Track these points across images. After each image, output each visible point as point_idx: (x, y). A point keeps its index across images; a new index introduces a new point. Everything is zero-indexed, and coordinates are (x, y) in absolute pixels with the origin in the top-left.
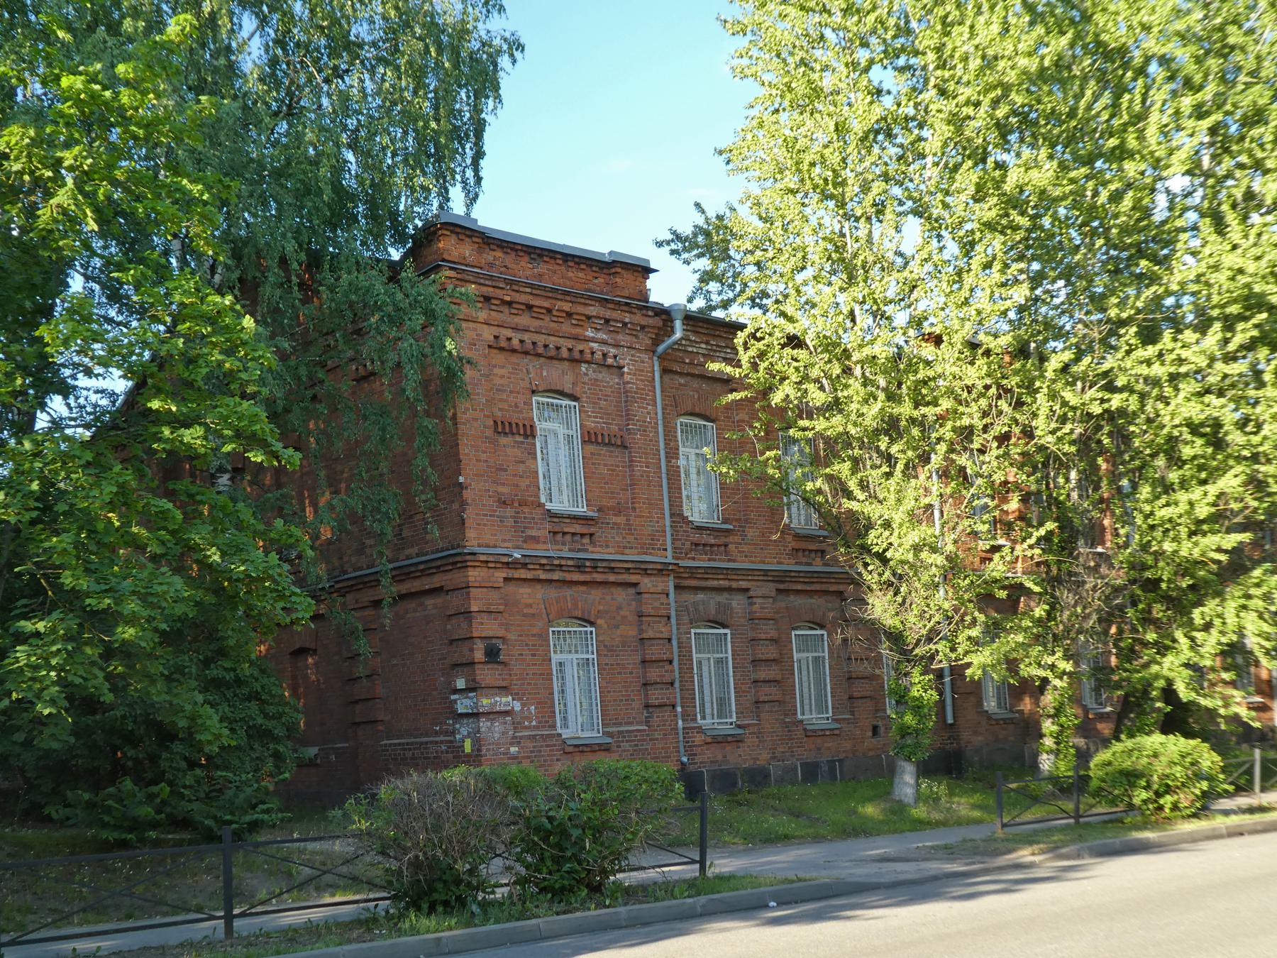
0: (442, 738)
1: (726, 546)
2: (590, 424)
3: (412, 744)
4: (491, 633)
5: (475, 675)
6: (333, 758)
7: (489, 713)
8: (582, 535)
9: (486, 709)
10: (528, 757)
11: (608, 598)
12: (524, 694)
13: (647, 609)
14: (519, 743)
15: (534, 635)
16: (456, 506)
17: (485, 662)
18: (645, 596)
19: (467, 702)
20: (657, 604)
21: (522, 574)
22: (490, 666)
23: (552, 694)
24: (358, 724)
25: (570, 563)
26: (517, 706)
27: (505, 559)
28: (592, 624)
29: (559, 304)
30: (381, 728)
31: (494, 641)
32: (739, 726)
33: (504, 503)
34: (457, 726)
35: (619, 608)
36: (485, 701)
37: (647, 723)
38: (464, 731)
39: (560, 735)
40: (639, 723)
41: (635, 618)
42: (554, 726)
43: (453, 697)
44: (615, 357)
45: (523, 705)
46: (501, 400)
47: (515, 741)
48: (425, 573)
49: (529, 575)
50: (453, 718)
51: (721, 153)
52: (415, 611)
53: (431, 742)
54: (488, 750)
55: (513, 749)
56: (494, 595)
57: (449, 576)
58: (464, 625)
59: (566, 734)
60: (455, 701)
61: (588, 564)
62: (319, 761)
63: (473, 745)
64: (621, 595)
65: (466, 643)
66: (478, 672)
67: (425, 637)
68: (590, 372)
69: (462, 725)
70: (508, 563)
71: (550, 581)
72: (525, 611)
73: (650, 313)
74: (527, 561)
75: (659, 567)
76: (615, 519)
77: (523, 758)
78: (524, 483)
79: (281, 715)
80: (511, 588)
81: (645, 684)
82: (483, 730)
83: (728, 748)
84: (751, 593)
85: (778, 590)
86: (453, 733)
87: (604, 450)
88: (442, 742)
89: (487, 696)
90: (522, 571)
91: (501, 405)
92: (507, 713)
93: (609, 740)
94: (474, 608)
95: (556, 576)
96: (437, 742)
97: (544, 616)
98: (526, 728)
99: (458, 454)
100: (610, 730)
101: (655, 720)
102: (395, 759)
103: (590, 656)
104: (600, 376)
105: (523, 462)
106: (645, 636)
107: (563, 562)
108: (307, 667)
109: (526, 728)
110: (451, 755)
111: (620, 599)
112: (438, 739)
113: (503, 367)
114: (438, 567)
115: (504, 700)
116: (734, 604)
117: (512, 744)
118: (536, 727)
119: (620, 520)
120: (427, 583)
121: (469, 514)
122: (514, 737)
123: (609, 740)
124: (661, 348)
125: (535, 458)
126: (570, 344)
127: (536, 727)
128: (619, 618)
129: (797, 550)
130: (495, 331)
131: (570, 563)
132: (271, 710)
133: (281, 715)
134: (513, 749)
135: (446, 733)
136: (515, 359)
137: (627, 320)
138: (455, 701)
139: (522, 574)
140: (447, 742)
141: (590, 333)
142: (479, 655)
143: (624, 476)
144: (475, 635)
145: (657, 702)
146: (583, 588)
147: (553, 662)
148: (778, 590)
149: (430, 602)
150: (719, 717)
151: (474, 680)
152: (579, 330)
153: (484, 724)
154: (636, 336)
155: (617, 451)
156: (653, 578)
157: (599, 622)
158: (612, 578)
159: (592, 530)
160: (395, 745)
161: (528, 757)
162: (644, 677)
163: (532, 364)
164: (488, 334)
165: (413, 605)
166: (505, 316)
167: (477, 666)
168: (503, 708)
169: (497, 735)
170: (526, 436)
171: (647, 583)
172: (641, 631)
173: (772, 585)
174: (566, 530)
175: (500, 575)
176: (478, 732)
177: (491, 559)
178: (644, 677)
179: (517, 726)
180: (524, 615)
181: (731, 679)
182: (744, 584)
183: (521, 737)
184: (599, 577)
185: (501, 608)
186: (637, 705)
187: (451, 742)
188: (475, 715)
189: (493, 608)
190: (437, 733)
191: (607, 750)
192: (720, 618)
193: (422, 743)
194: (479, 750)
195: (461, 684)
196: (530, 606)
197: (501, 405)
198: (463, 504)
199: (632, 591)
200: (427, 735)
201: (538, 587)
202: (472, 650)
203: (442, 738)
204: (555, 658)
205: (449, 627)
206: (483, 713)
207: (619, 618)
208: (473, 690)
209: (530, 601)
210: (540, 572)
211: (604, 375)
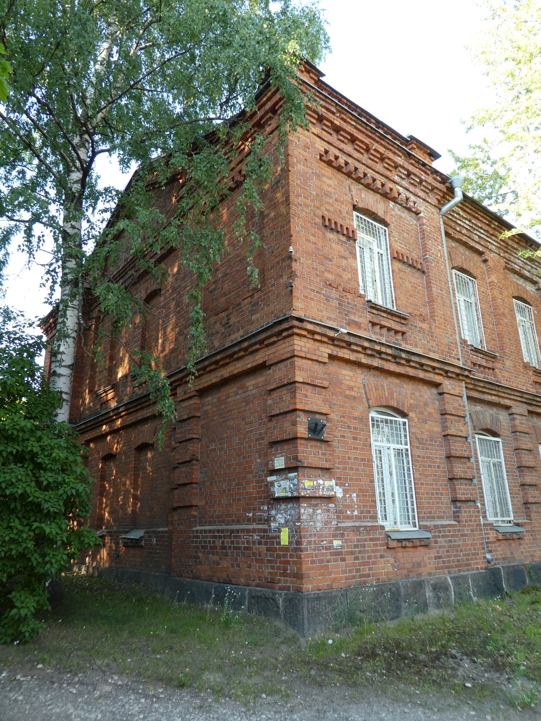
0: (254, 526)
1: (493, 369)
2: (397, 247)
3: (222, 531)
4: (315, 408)
5: (296, 451)
6: (154, 540)
7: (311, 498)
8: (396, 332)
9: (308, 493)
10: (352, 553)
11: (417, 394)
12: (346, 479)
13: (450, 408)
14: (342, 535)
15: (355, 418)
16: (284, 280)
17: (308, 439)
18: (446, 395)
19: (286, 484)
20: (456, 405)
21: (345, 354)
22: (312, 443)
23: (373, 481)
24: (175, 509)
25: (389, 351)
26: (339, 492)
27: (331, 334)
28: (404, 415)
29: (376, 146)
30: (194, 513)
31: (318, 416)
32: (518, 525)
33: (330, 285)
34: (273, 512)
35: (426, 404)
36: (308, 483)
37: (456, 517)
38: (281, 519)
39: (383, 527)
40: (448, 518)
41: (437, 416)
42: (374, 518)
43: (270, 479)
44: (415, 203)
45: (345, 491)
46: (328, 203)
47: (339, 533)
48: (249, 352)
49: (353, 357)
50: (269, 504)
51: (463, 123)
52: (236, 394)
53: (243, 530)
54: (309, 543)
55: (337, 543)
56: (316, 367)
57: (272, 349)
58: (287, 397)
59: (388, 526)
60: (272, 484)
61: (403, 355)
62: (143, 543)
63: (291, 536)
64: (428, 393)
65: (288, 416)
66: (300, 448)
67: (244, 419)
68: (396, 209)
69: (278, 511)
70: (332, 339)
71: (369, 367)
72: (347, 392)
73: (439, 178)
74: (352, 340)
75: (457, 371)
76: (420, 324)
77: (348, 553)
78: (346, 276)
79: (59, 485)
80: (334, 367)
81: (451, 479)
82: (304, 517)
83: (513, 545)
84: (513, 410)
85: (530, 412)
86: (268, 521)
87: (408, 270)
88: (254, 531)
89: (309, 478)
90: (346, 351)
91: (328, 207)
92: (329, 499)
93: (428, 535)
94: (299, 378)
95: (376, 362)
96: (248, 531)
97: (365, 400)
98: (348, 518)
99: (289, 229)
100: (428, 523)
101: (464, 515)
102: (204, 547)
103: (403, 447)
104: (403, 215)
105: (346, 259)
106: (450, 432)
107: (383, 349)
108: (146, 460)
109: (348, 518)
110: (264, 547)
111: (426, 397)
112: (250, 527)
113: (331, 179)
114: (261, 342)
115: (327, 483)
116: (501, 417)
117: (335, 536)
118: (358, 518)
119: (425, 326)
120: (249, 362)
121: (297, 284)
122: (338, 528)
123: (428, 535)
124: (445, 209)
125: (355, 258)
126: (383, 180)
127: (358, 518)
128: (426, 414)
129: (536, 382)
130: (327, 147)
131: (389, 351)
132: (47, 477)
133: (59, 485)
134: (337, 543)
135: (260, 520)
136: (340, 176)
137: (423, 178)
138: (272, 484)
139: (345, 354)
140: (260, 530)
141: (396, 178)
142: (302, 430)
143: (424, 295)
144: (299, 406)
145: (463, 497)
146: (396, 381)
147: (373, 448)
148: (530, 412)
149: (251, 383)
150: (502, 516)
151: (296, 458)
152: (388, 173)
153: (305, 510)
154: (427, 193)
155: (418, 274)
156: (451, 381)
157: (412, 414)
158: (421, 374)
159: (404, 329)
160: (206, 531)
161: (352, 553)
162: (451, 471)
163: (356, 188)
164: (321, 146)
165: (235, 389)
166: (334, 138)
167: (299, 441)
168: (326, 493)
169: (319, 525)
170: (349, 238)
171: (448, 385)
172: (445, 428)
173: (525, 406)
174: (383, 323)
175: (325, 350)
176: (299, 520)
177: (318, 329)
178: (451, 471)
179: (340, 515)
180: (346, 397)
181: (506, 482)
182: (508, 402)
183: (345, 529)
184: (411, 372)
185: (326, 384)
186: (446, 499)
187: (265, 531)
188: (296, 499)
189: (317, 382)
190: (249, 521)
191: (426, 546)
192: (494, 429)
193: (232, 531)
194: (299, 543)
195: (279, 463)
196: (351, 388)
197: (328, 207)
198: (292, 275)
199: (434, 391)
200: (239, 522)
201: (359, 371)
202: (294, 423)
203: (254, 526)
204: (374, 445)
205: (270, 402)
206: (303, 497)
207: (426, 414)
208: (294, 469)
209: (352, 384)
210: (362, 356)
211: (405, 214)
